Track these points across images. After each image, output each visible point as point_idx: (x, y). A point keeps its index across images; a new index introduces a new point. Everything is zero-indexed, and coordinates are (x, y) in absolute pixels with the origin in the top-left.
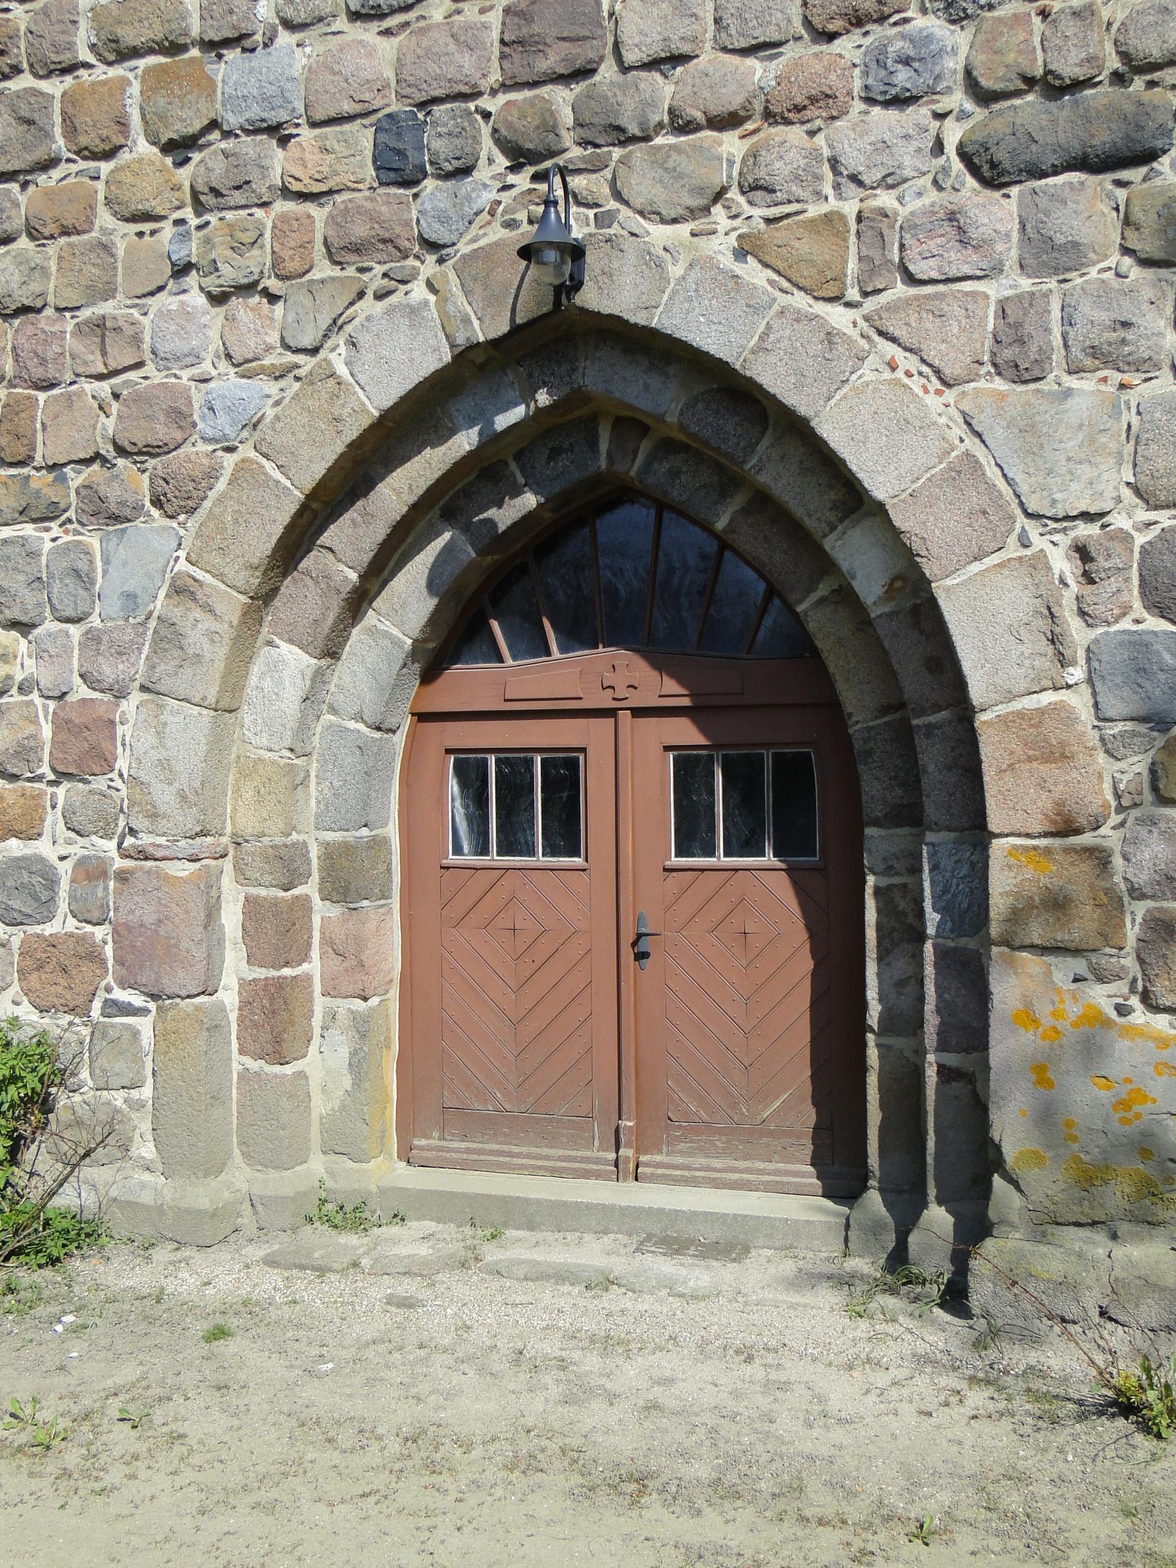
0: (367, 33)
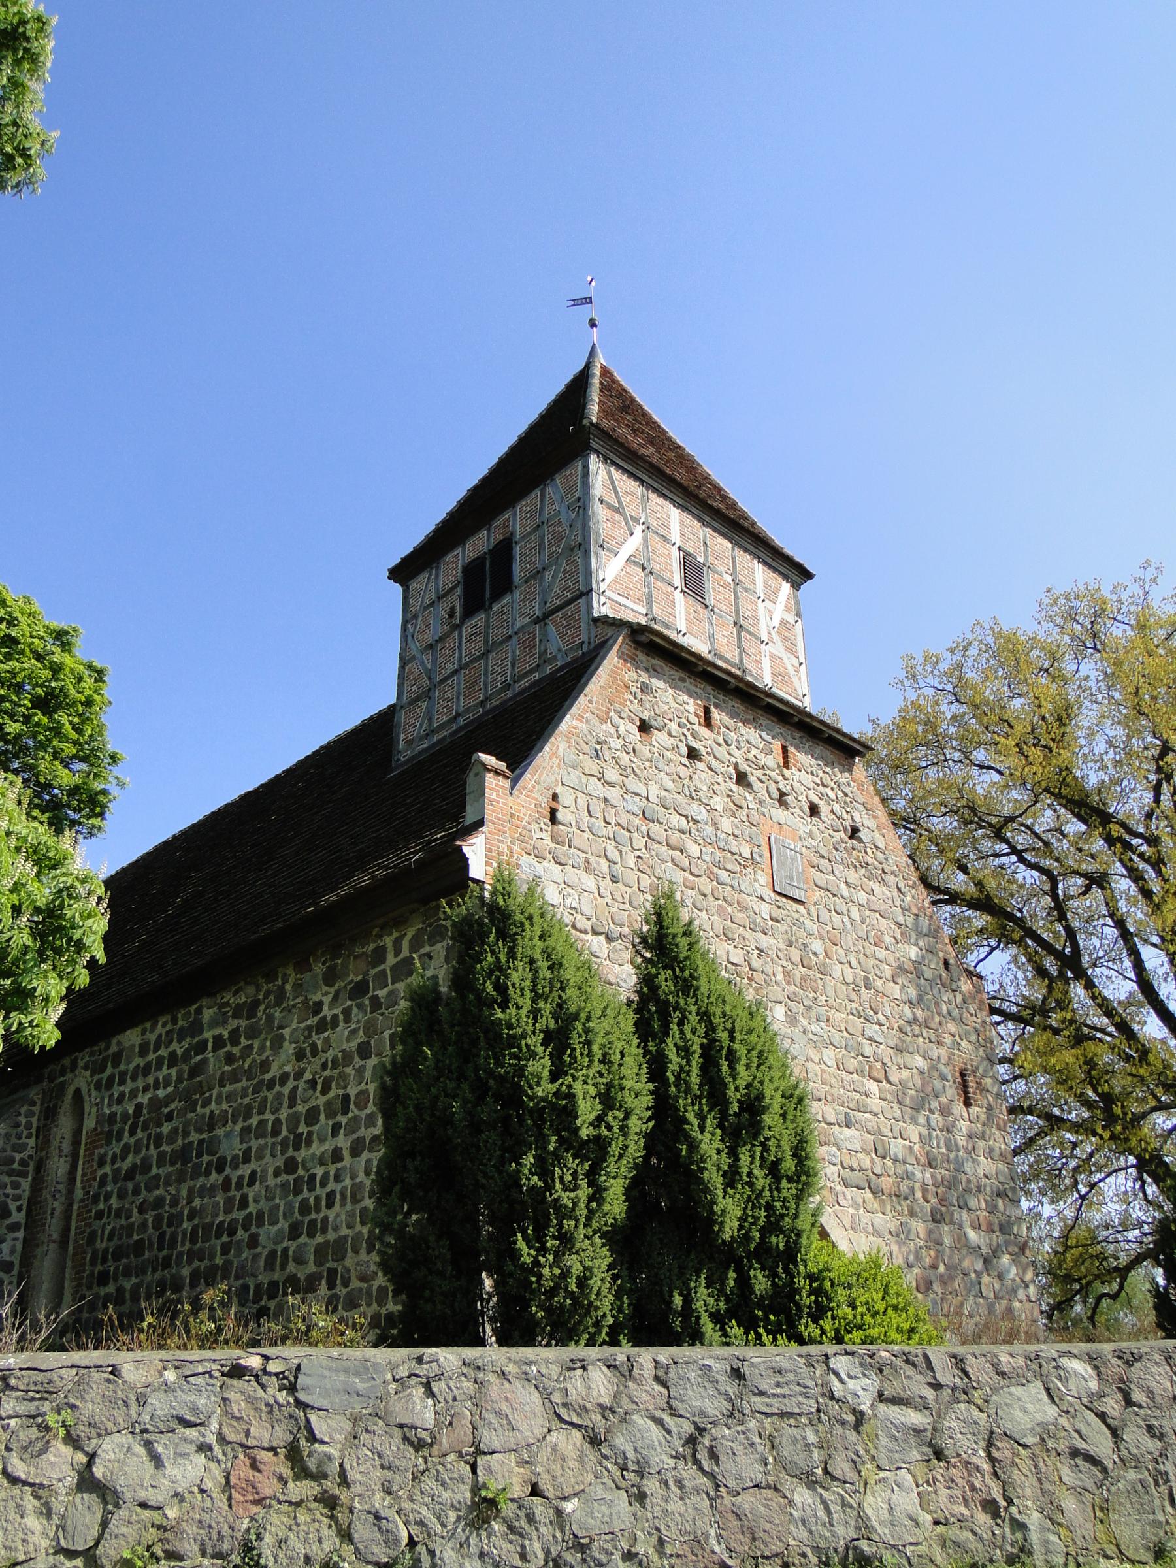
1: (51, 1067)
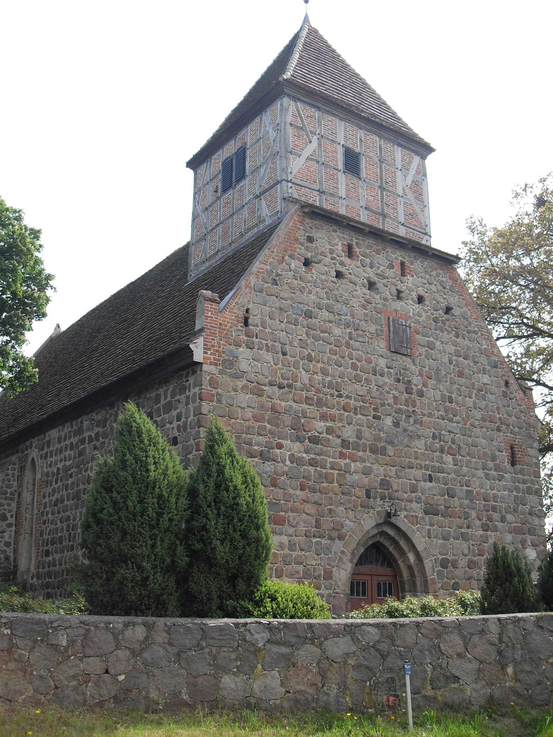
0: (364, 476)
1: (22, 445)
